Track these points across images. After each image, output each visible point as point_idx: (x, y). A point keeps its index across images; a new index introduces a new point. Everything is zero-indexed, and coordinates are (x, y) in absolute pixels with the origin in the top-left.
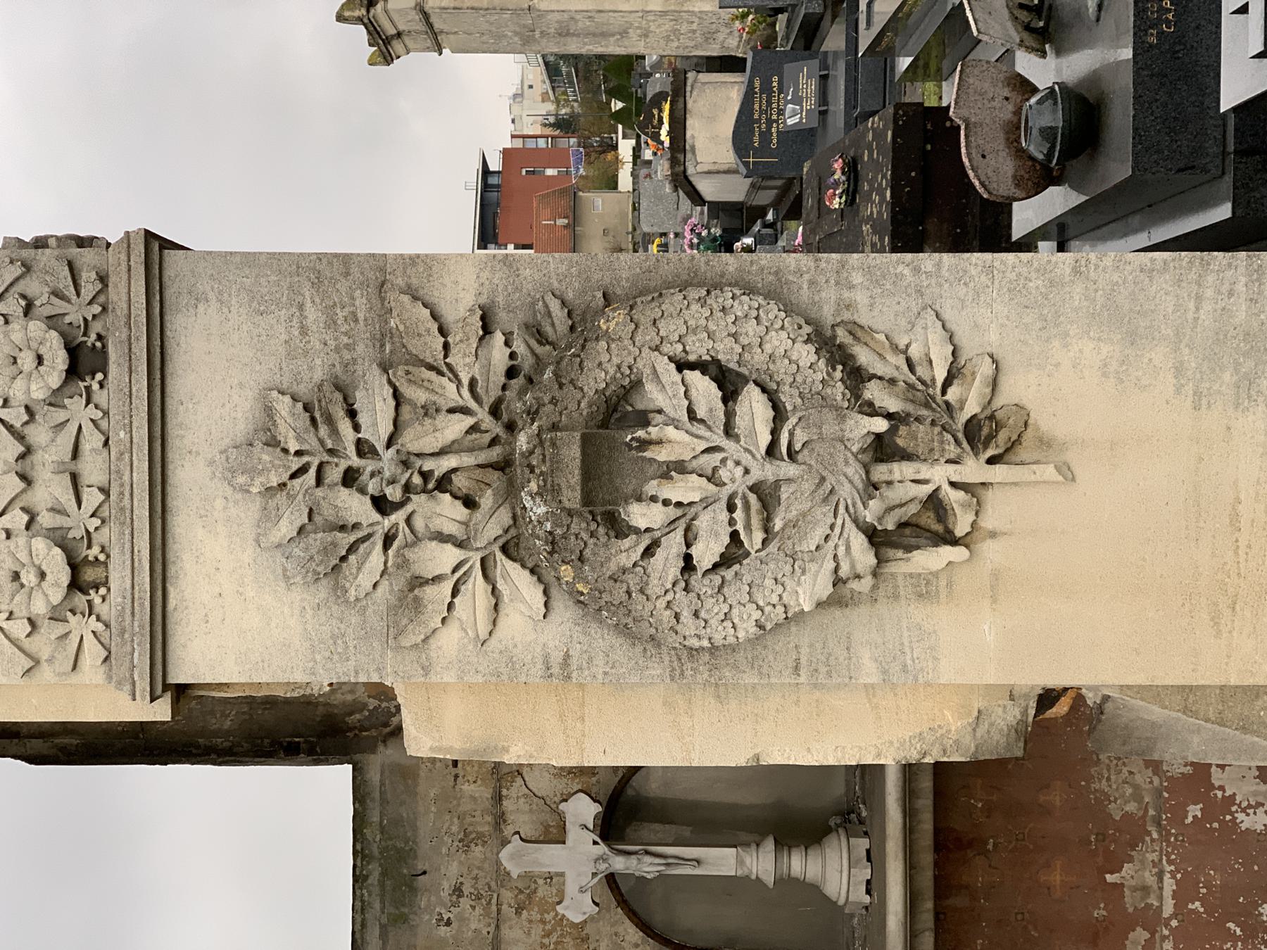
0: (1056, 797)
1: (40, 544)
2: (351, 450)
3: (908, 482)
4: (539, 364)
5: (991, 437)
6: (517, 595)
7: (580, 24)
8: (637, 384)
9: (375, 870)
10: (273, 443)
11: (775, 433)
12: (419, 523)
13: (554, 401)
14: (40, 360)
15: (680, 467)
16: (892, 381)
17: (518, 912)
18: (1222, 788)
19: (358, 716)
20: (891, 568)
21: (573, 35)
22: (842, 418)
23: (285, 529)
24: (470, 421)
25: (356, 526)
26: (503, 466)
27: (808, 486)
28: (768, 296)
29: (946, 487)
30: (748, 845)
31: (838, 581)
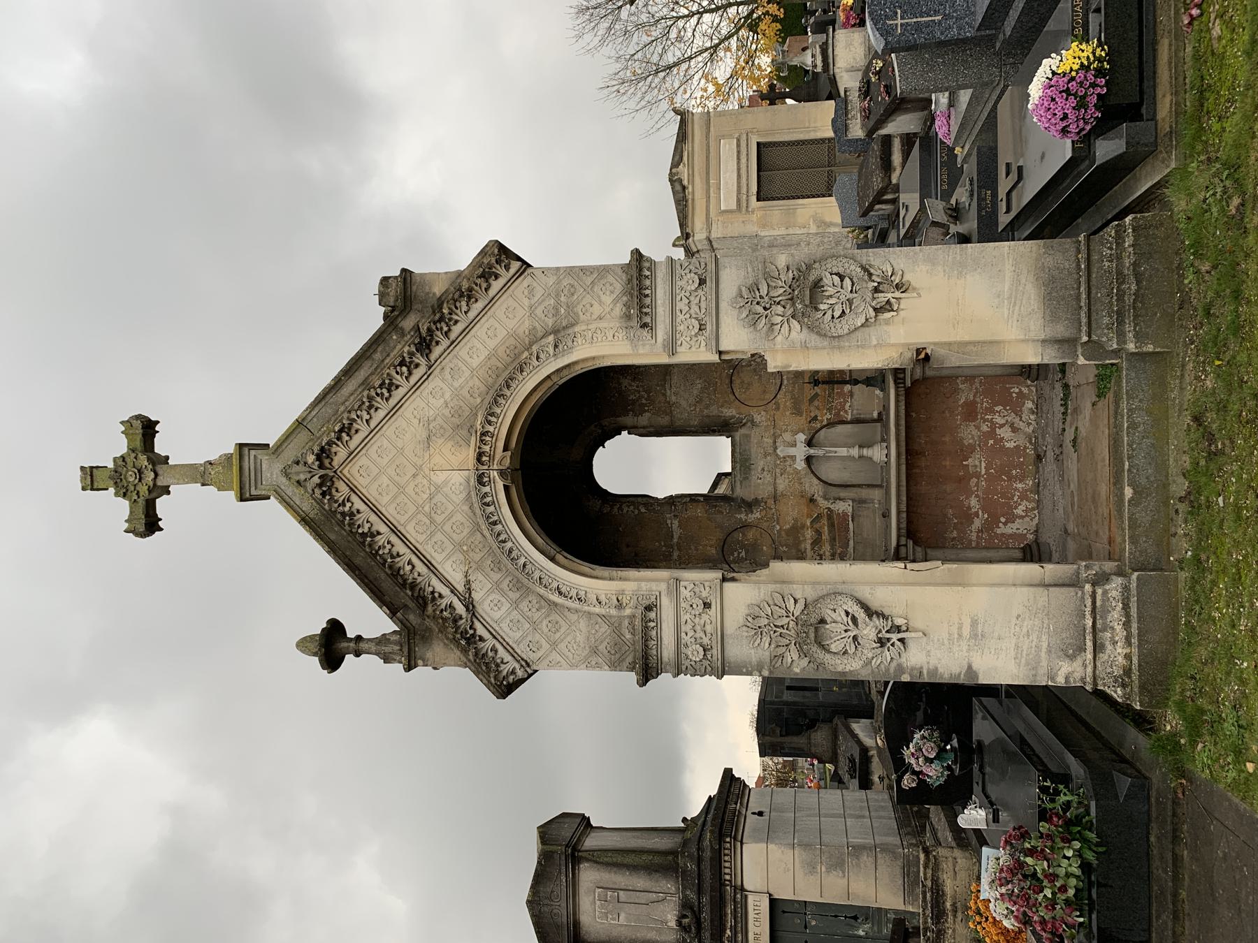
3: (882, 298)
9: (738, 466)
23: (744, 315)
26: (791, 299)
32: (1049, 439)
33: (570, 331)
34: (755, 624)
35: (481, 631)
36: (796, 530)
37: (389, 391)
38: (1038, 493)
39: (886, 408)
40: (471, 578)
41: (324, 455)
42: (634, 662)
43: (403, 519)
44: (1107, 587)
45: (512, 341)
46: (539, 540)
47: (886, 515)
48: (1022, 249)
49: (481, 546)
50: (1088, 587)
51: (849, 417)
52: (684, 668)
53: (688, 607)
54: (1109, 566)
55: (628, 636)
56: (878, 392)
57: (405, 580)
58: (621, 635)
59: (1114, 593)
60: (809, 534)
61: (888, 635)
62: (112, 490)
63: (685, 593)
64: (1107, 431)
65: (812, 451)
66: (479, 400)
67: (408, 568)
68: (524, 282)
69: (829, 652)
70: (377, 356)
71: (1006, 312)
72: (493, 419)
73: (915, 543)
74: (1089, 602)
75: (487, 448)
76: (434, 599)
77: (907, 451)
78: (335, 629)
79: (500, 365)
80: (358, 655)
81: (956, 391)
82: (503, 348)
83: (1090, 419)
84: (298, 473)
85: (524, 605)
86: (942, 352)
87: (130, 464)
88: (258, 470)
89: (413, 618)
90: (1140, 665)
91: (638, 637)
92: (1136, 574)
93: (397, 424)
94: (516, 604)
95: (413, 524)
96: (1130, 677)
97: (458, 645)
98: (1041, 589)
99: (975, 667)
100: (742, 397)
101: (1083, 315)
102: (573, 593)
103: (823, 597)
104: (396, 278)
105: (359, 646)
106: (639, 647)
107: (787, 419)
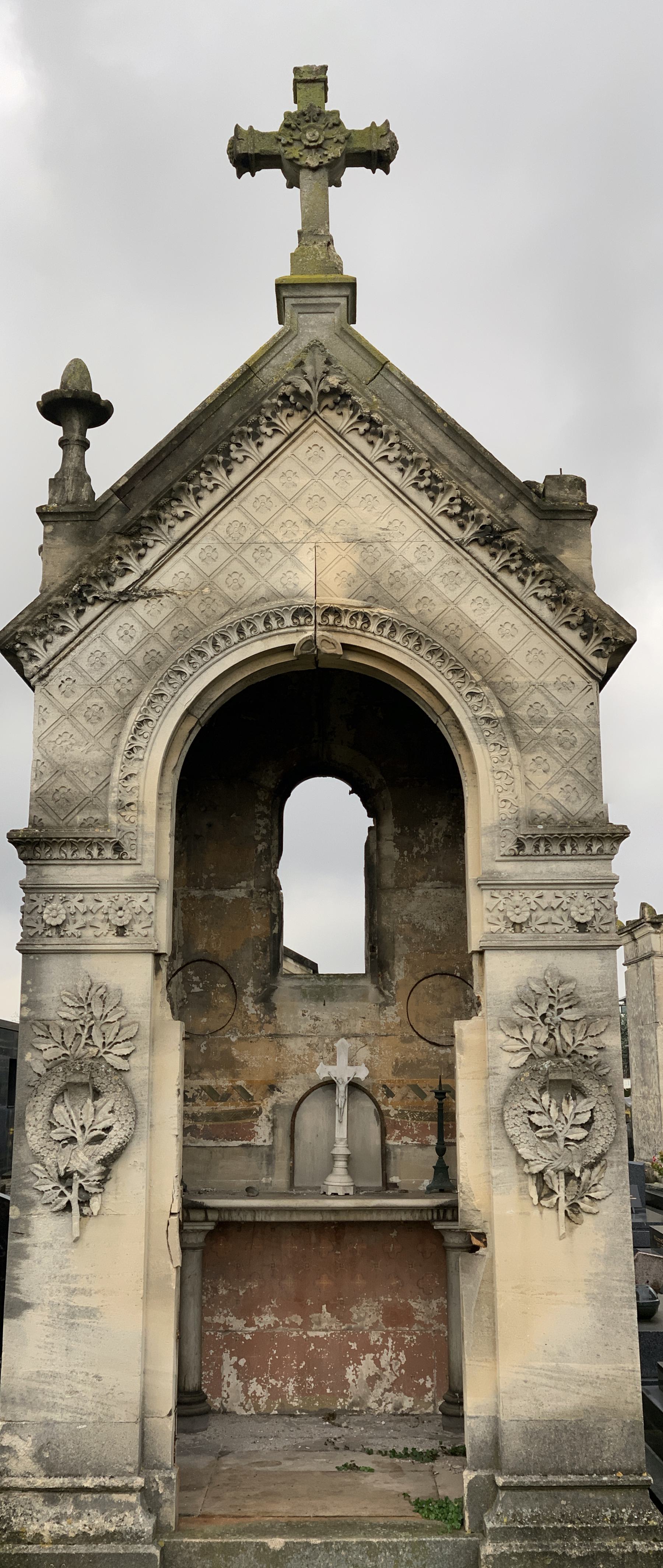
0: (359, 1282)
1: (528, 914)
2: (560, 1007)
3: (558, 1183)
4: (589, 1065)
5: (573, 1211)
6: (517, 1058)
7: (648, 1055)
8: (585, 1097)
10: (561, 983)
11: (573, 1140)
12: (538, 1028)
13: (580, 1070)
14: (582, 914)
15: (560, 1110)
16: (590, 1179)
17: (309, 1045)
18: (364, 1359)
19: (388, 976)
20: (530, 1178)
21: (642, 1050)
22: (579, 1162)
23: (534, 986)
24: (571, 1044)
25: (537, 1008)
26: (557, 1054)
27: (557, 1151)
28: (614, 1139)
29: (557, 1197)
30: (347, 1143)
31: (527, 1161)
32: (357, 1431)
33: (510, 741)
34: (94, 999)
35: (91, 612)
36: (230, 1065)
37: (427, 488)
38: (281, 1414)
39: (404, 1194)
40: (165, 599)
41: (339, 398)
42: (42, 827)
43: (248, 505)
44: (139, 1510)
45: (495, 659)
46: (216, 694)
47: (250, 1192)
48: (630, 1389)
49: (210, 612)
50: (139, 1482)
51: (390, 1142)
52: (33, 896)
53: (119, 904)
54: (170, 1514)
55: (79, 819)
56: (427, 1183)
57: (163, 508)
58: (81, 808)
59: (129, 1520)
60: (224, 1083)
61: (75, 1187)
62: (294, 108)
63: (139, 900)
64: (364, 1513)
65: (342, 1089)
66: (413, 611)
67: (180, 512)
68: (578, 677)
69: (54, 1102)
70: (475, 473)
71: (538, 1364)
72: (387, 631)
73: (210, 1234)
74: (117, 1482)
75: (346, 621)
76: (137, 547)
77: (342, 1224)
78: (98, 412)
79: (462, 641)
80: (63, 443)
81: (428, 1296)
82: (487, 647)
83: (384, 1490)
84: (313, 363)
85: (125, 672)
86: (481, 1269)
87: (329, 133)
88: (318, 309)
89: (111, 519)
90: (25, 1555)
91: (77, 833)
92: (157, 1553)
93: (381, 498)
94: (126, 661)
95: (242, 519)
96: (8, 1541)
97: (72, 581)
98: (137, 1412)
99: (28, 1314)
100: (420, 989)
101: (535, 1478)
102: (141, 742)
103: (131, 1096)
104: (584, 499)
105: (75, 445)
106: (64, 834)
107: (390, 1053)
